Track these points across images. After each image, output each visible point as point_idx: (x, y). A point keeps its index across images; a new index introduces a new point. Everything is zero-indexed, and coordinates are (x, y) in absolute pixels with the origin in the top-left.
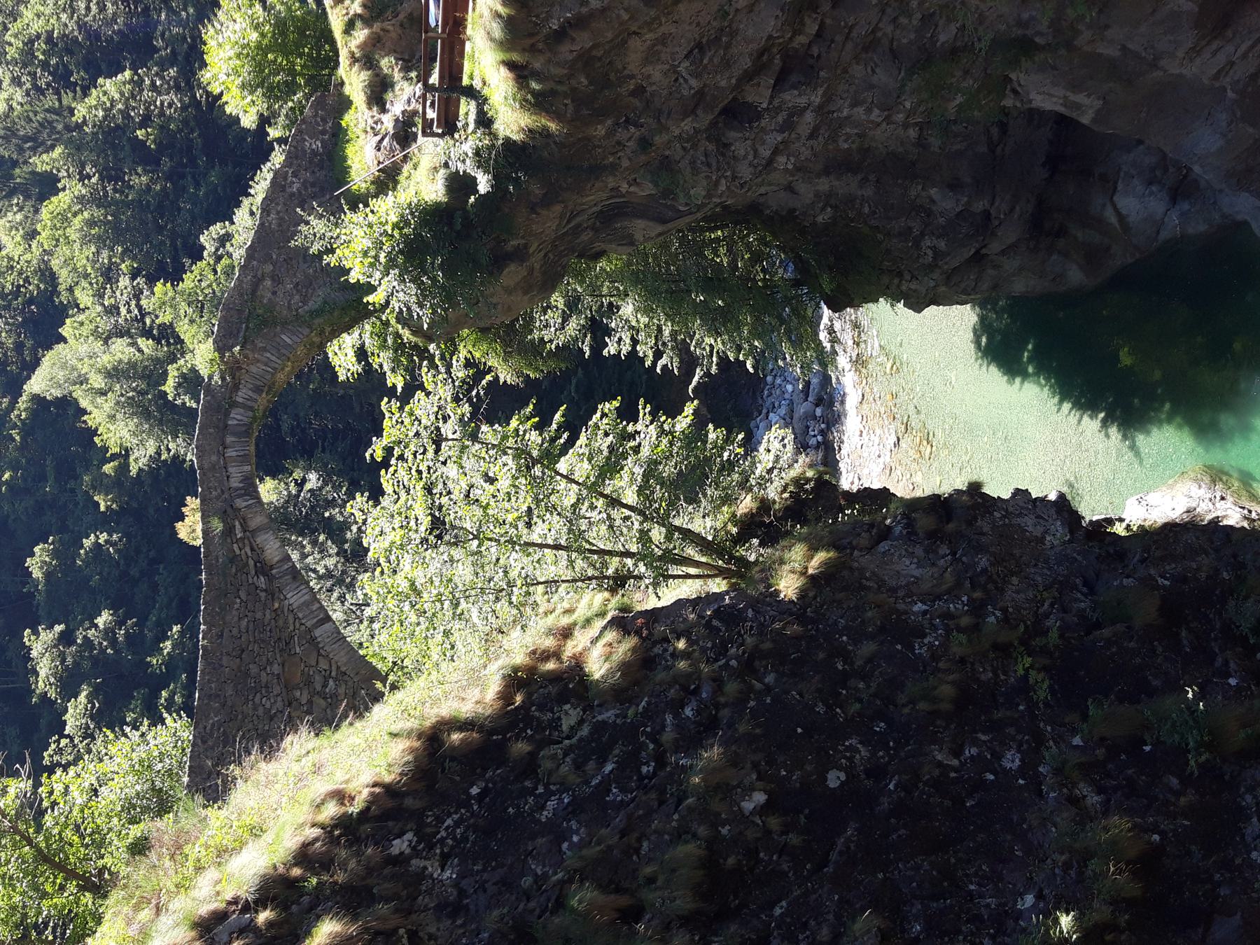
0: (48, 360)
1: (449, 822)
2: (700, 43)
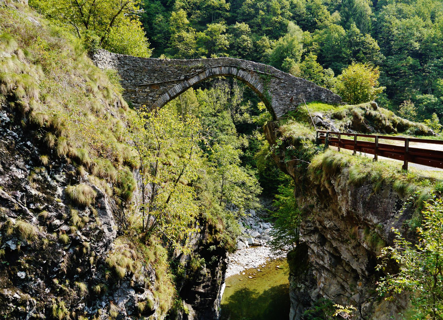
0: (297, 27)
1: (15, 134)
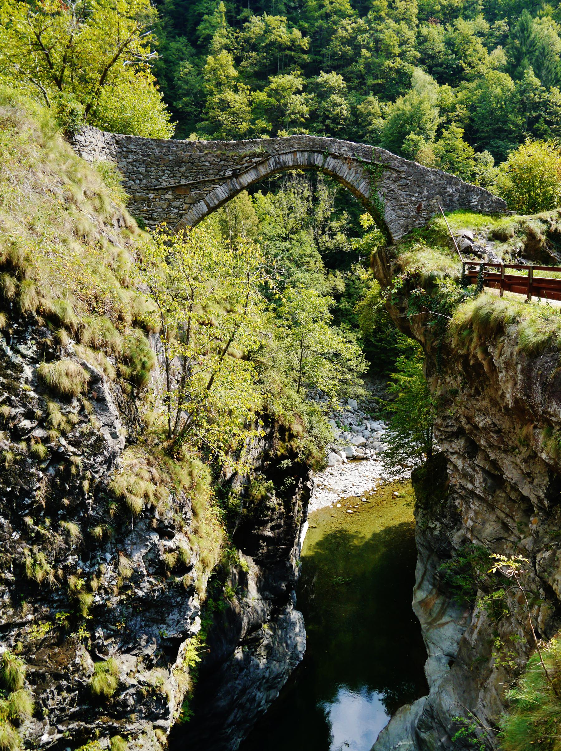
2: (501, 432)
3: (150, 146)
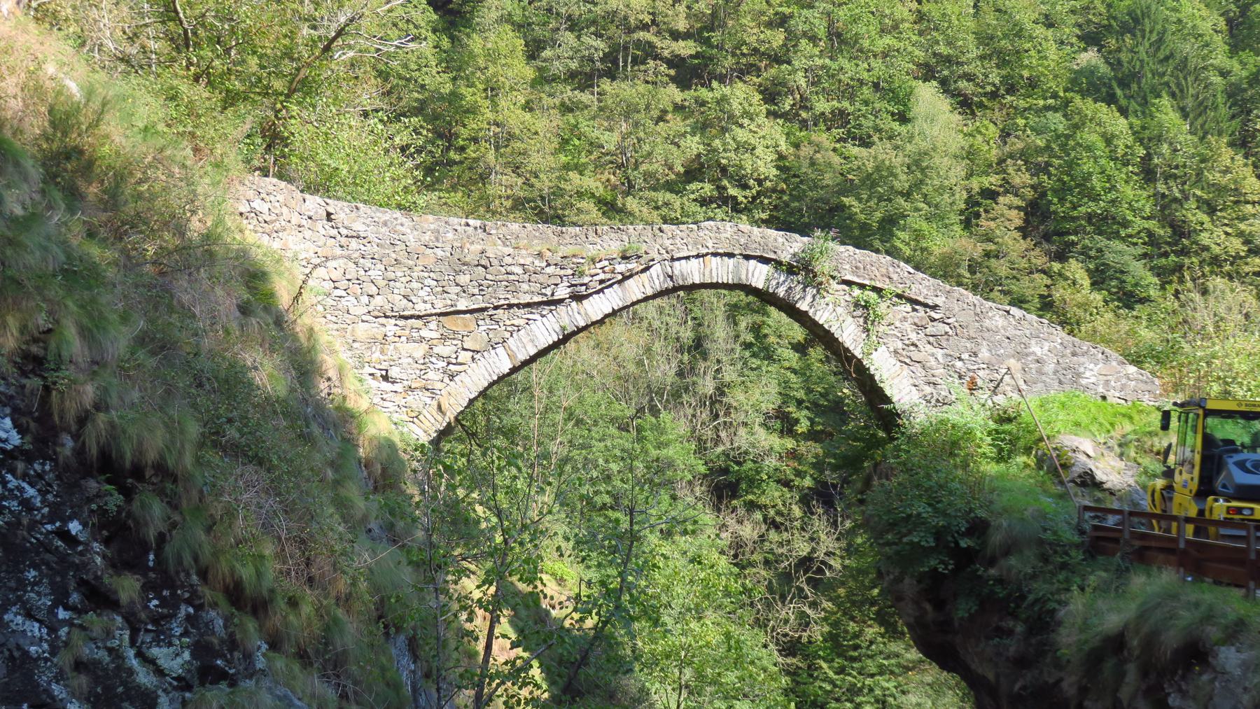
1: (31, 492)
3: (399, 227)
